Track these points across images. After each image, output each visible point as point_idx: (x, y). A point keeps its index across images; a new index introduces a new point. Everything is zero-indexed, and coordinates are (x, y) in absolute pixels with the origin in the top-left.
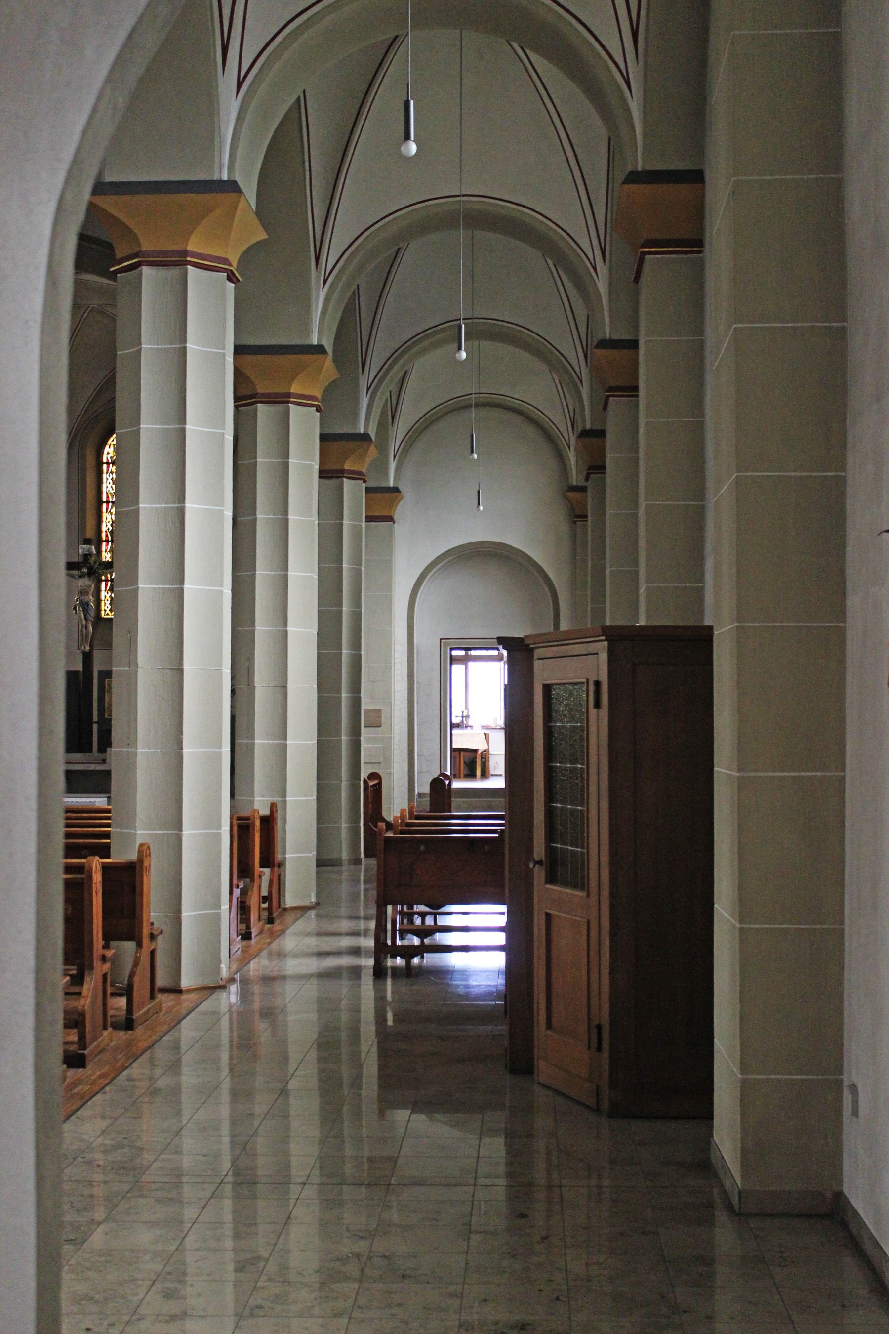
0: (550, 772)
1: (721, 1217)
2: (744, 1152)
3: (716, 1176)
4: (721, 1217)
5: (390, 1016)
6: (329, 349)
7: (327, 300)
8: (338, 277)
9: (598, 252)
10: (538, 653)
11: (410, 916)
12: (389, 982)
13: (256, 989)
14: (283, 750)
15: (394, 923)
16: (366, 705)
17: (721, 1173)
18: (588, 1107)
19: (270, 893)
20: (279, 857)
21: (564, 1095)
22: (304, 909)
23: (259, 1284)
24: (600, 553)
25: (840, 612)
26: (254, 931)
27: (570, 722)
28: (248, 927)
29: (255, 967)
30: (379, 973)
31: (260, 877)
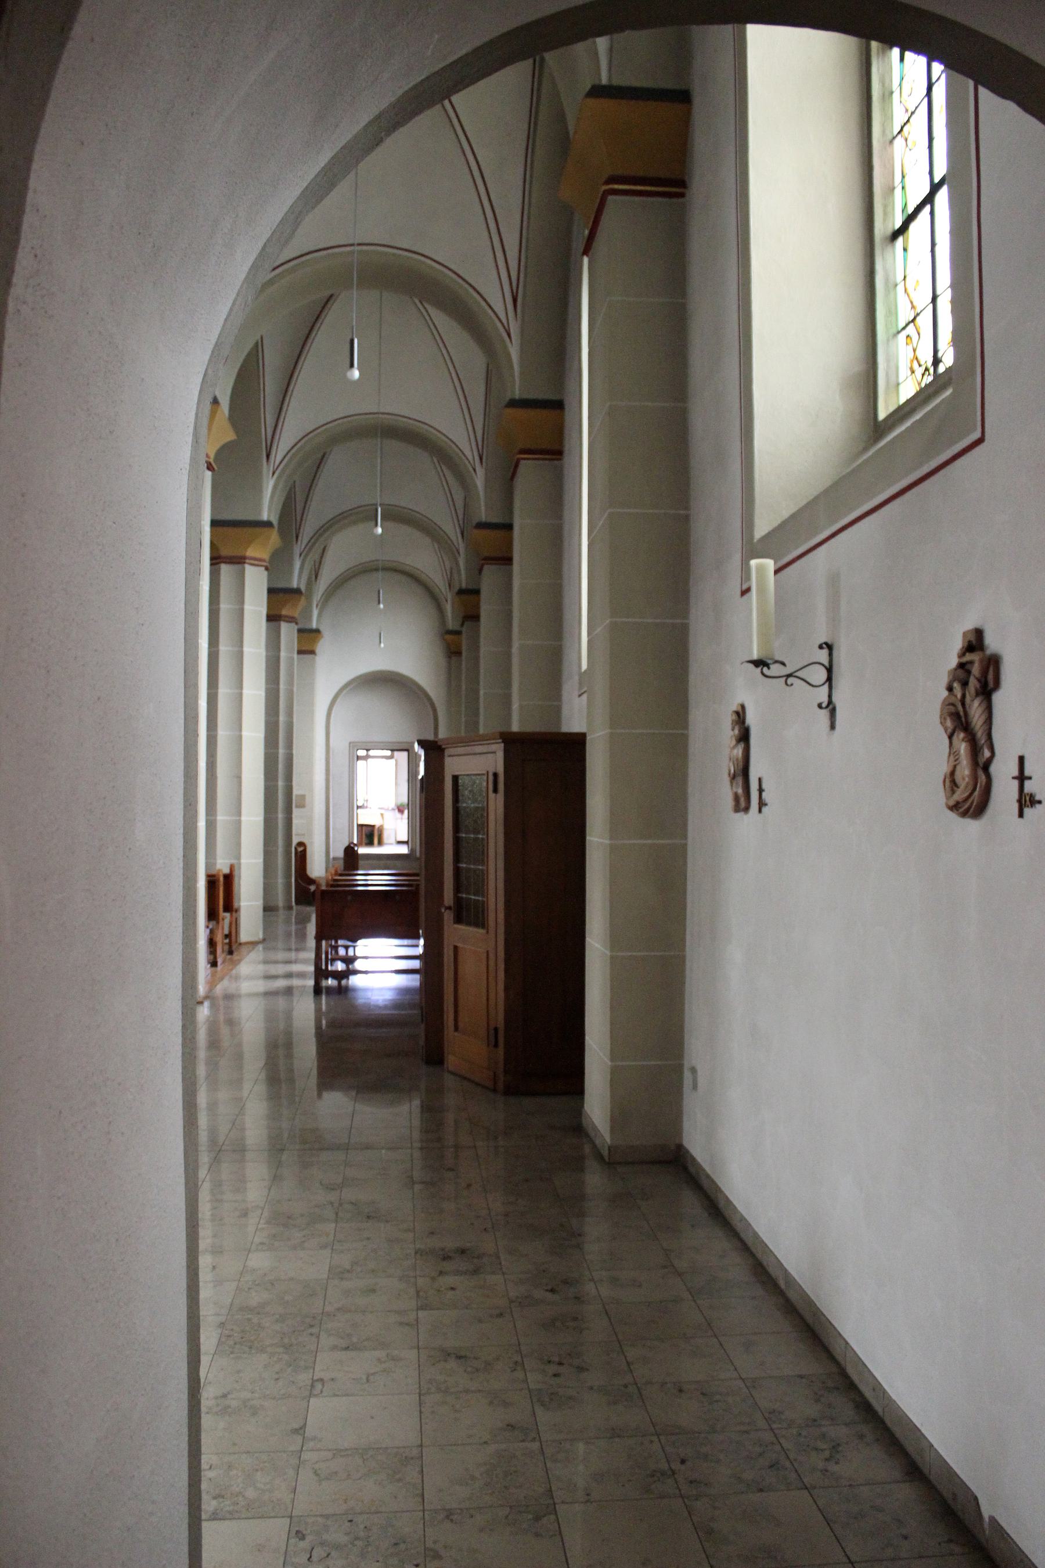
0: (457, 841)
1: (591, 1164)
2: (613, 1120)
3: (587, 1135)
4: (591, 1164)
5: (324, 1022)
6: (275, 522)
7: (275, 487)
8: (283, 471)
9: (477, 458)
10: (447, 752)
11: (336, 948)
12: (324, 997)
13: (221, 1003)
14: (238, 824)
15: (327, 953)
16: (296, 791)
17: (592, 1134)
18: (487, 1088)
19: (230, 932)
20: (236, 905)
21: (469, 1080)
22: (253, 944)
23: (260, 1226)
24: (475, 679)
25: (685, 724)
26: (220, 961)
27: (474, 803)
28: (215, 958)
29: (219, 989)
30: (318, 990)
31: (223, 919)
